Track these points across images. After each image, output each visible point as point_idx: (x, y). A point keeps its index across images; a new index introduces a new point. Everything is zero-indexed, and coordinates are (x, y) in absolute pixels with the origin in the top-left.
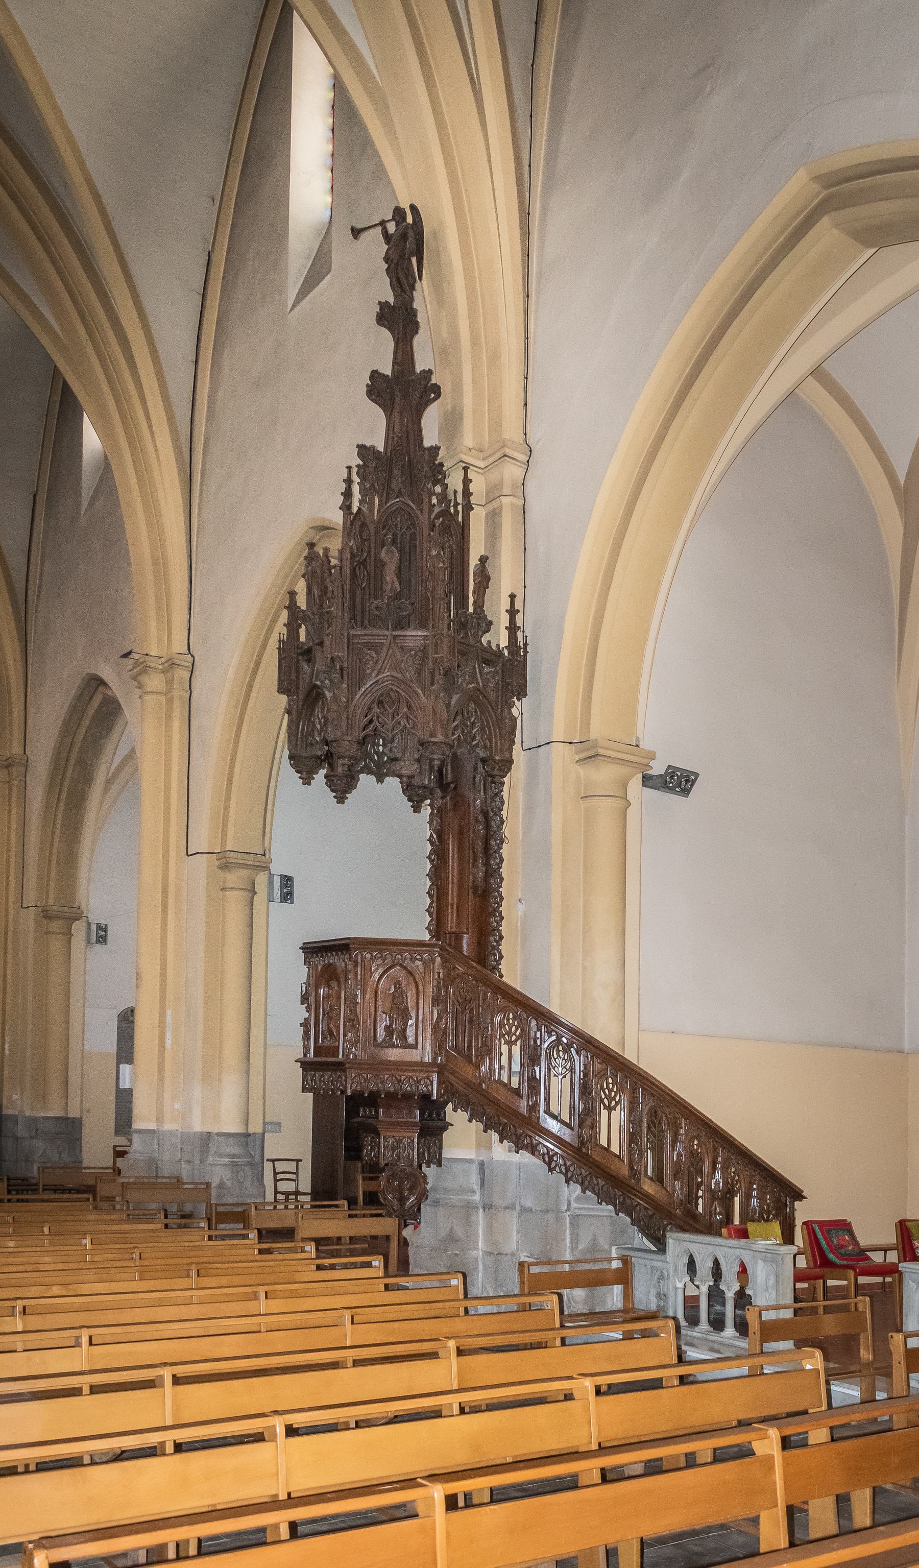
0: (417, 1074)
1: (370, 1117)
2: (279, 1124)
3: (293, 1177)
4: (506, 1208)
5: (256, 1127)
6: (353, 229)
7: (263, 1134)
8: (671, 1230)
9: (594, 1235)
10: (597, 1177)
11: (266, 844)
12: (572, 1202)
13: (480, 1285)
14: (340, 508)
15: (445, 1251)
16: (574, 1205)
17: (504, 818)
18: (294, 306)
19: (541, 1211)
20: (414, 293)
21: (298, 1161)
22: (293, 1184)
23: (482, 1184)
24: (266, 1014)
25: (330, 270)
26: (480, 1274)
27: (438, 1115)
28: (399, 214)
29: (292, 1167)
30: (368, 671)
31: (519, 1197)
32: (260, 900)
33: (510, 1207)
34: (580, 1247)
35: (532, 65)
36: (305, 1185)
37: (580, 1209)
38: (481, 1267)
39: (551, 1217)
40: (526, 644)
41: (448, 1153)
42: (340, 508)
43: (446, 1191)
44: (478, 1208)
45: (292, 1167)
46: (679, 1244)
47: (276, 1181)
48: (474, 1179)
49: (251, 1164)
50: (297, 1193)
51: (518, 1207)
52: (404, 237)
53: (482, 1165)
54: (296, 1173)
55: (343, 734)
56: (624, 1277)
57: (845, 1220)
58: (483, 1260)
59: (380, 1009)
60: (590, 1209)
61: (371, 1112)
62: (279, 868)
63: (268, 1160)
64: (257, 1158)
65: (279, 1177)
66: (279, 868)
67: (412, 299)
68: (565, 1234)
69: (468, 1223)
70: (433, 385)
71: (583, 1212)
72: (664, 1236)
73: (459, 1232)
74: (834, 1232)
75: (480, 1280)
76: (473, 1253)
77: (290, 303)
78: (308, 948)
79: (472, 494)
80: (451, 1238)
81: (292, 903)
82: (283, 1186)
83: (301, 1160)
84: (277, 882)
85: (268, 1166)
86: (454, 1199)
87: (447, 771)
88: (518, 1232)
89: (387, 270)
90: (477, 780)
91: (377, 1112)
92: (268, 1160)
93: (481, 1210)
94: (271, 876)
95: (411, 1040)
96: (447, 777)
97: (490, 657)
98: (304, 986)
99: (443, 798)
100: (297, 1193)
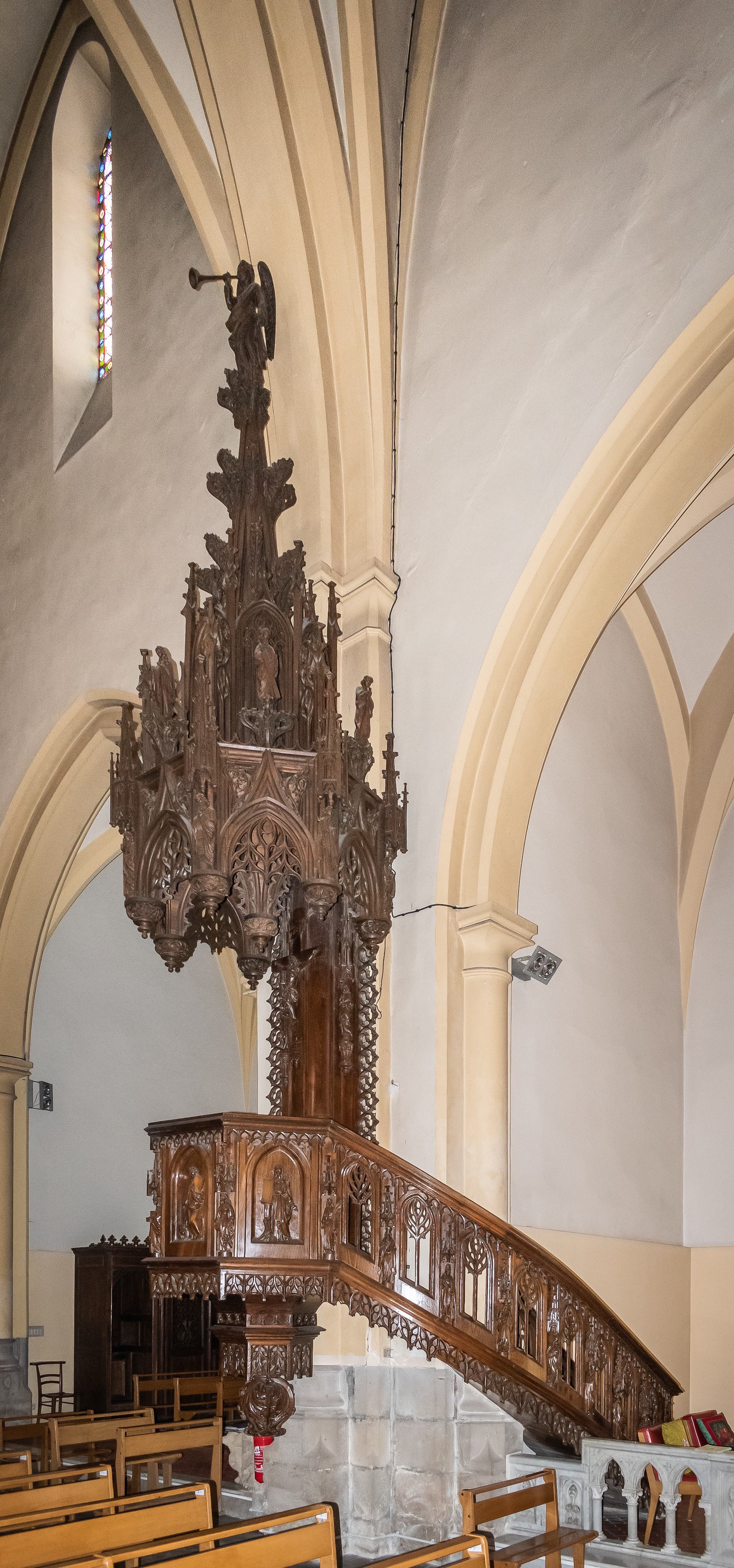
0: (264, 1273)
1: (232, 1324)
2: (41, 1327)
3: (57, 1379)
4: (382, 1417)
5: (20, 1332)
6: (193, 273)
7: (27, 1338)
8: (585, 1437)
9: (488, 1444)
10: (517, 1385)
11: (26, 1051)
12: (458, 1408)
13: (350, 1501)
14: (182, 613)
15: (316, 1469)
16: (460, 1412)
17: (378, 989)
18: (60, 465)
19: (426, 1421)
20: (265, 372)
21: (61, 1363)
22: (58, 1385)
23: (352, 1392)
24: (28, 1221)
25: (110, 416)
26: (350, 1491)
27: (310, 1319)
28: (245, 269)
29: (55, 1369)
30: (240, 794)
31: (395, 1405)
32: (20, 1104)
33: (385, 1417)
34: (473, 1458)
35: (402, 123)
36: (69, 1386)
37: (471, 1416)
38: (351, 1483)
39: (439, 1427)
40: (405, 793)
41: (318, 1360)
42: (182, 613)
43: (311, 1401)
44: (347, 1418)
45: (55, 1369)
46: (597, 1453)
47: (40, 1384)
48: (341, 1387)
49: (17, 1369)
50: (61, 1395)
51: (392, 1416)
52: (253, 299)
53: (350, 1373)
54: (60, 1375)
55: (209, 867)
56: (548, 1494)
57: (713, 1412)
58: (354, 1474)
59: (258, 1198)
60: (481, 1416)
61: (233, 1318)
62: (38, 1075)
63: (31, 1364)
64: (21, 1363)
65: (43, 1380)
66: (38, 1075)
67: (234, 416)
68: (453, 1444)
69: (339, 1438)
70: (287, 485)
71: (474, 1420)
72: (579, 1444)
73: (329, 1447)
74: (715, 1425)
75: (350, 1496)
76: (343, 1468)
77: (56, 463)
78: (155, 1129)
79: (339, 616)
80: (321, 1454)
81: (51, 1110)
82: (47, 1389)
83: (64, 1363)
84: (36, 1088)
85: (32, 1370)
86: (321, 1410)
87: (305, 936)
88: (394, 1442)
89: (230, 339)
90: (343, 948)
91: (243, 1319)
92: (31, 1364)
93: (350, 1421)
94: (30, 1083)
95: (294, 1236)
96: (305, 943)
97: (370, 800)
98: (151, 1174)
99: (301, 967)
100: (61, 1395)
